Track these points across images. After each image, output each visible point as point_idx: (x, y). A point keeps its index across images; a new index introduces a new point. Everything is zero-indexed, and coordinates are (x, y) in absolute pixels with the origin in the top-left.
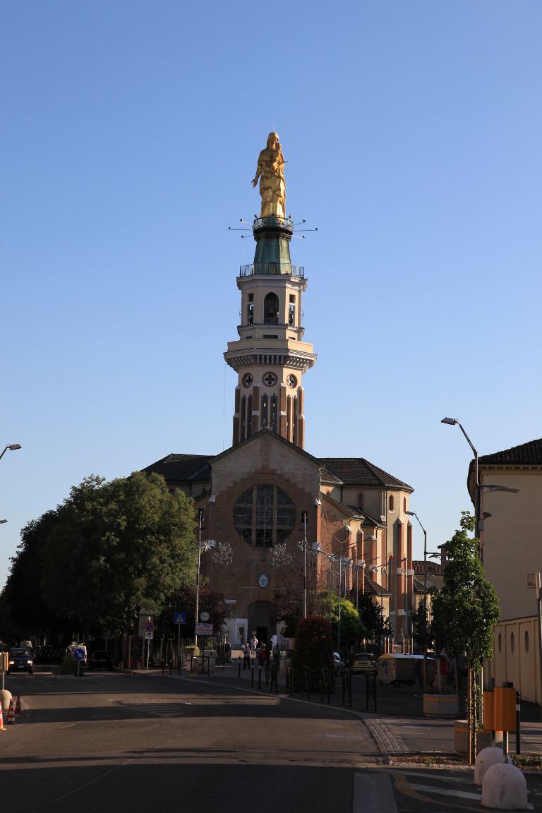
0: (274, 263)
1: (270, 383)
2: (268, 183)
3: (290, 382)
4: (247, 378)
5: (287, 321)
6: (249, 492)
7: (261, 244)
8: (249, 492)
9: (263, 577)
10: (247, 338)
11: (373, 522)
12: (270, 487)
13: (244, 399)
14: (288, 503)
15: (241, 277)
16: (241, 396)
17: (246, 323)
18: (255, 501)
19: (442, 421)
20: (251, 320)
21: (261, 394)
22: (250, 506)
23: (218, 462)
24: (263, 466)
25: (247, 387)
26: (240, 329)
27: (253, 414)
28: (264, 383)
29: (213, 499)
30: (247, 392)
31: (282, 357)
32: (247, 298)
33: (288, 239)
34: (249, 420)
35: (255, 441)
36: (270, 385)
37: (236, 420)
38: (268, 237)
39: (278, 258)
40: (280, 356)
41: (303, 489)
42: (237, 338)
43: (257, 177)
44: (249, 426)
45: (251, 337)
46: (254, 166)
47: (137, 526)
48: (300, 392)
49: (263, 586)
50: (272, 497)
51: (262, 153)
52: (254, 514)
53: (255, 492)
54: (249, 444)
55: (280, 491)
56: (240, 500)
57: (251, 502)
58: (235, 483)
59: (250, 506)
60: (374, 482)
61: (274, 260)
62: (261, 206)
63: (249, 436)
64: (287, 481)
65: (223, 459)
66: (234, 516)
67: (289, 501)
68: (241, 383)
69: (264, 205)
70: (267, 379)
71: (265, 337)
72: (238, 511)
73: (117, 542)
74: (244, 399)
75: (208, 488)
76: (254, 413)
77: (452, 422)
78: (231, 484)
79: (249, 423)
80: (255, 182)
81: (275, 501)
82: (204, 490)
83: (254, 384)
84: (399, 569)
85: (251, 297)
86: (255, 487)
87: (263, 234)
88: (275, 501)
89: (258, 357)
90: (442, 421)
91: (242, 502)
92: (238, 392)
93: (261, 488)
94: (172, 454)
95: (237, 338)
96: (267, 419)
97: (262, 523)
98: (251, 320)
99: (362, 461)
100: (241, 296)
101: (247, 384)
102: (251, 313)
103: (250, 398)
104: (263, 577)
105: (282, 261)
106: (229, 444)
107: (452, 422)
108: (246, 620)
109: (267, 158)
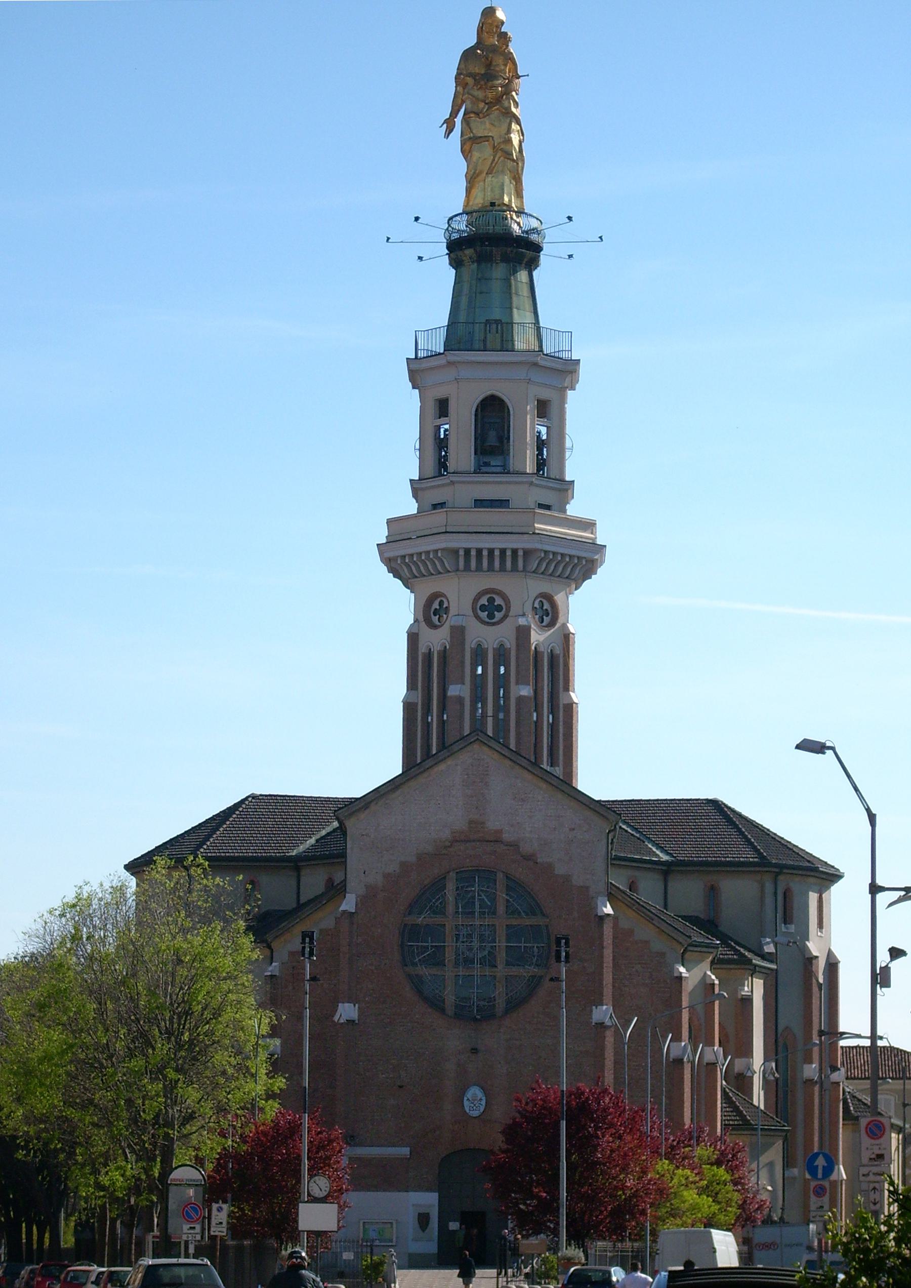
0: (498, 322)
1: (491, 616)
2: (481, 128)
3: (540, 613)
4: (436, 605)
5: (530, 467)
6: (438, 885)
7: (466, 277)
8: (438, 885)
9: (475, 1092)
10: (435, 506)
11: (744, 955)
12: (487, 875)
13: (429, 656)
14: (534, 914)
15: (416, 357)
16: (422, 649)
17: (430, 471)
18: (451, 909)
19: (798, 747)
20: (442, 465)
21: (470, 643)
22: (438, 919)
23: (362, 816)
24: (471, 822)
25: (435, 627)
26: (417, 488)
27: (449, 693)
28: (477, 617)
29: (349, 904)
30: (437, 639)
31: (521, 553)
32: (432, 410)
33: (532, 264)
34: (443, 708)
35: (449, 762)
36: (490, 622)
37: (409, 708)
38: (483, 259)
39: (509, 308)
40: (515, 552)
41: (567, 878)
42: (410, 507)
43: (454, 113)
44: (442, 724)
45: (442, 505)
46: (449, 88)
47: (548, 1197)
48: (567, 638)
49: (475, 1113)
50: (493, 899)
51: (468, 55)
52: (450, 942)
53: (451, 886)
54: (436, 769)
55: (513, 885)
56: (414, 907)
57: (441, 911)
58: (403, 864)
59: (438, 919)
60: (752, 857)
61: (496, 314)
62: (464, 184)
63: (442, 746)
64: (530, 858)
65: (373, 807)
66: (402, 946)
67: (535, 909)
68: (421, 618)
69: (472, 180)
70: (483, 608)
71: (480, 503)
72: (411, 933)
73: (22, 1151)
74: (429, 656)
75: (338, 877)
76: (454, 690)
77: (817, 748)
78: (393, 868)
79: (440, 716)
80: (449, 124)
81: (501, 909)
82: (330, 883)
83: (451, 620)
84: (806, 1067)
85: (442, 408)
86: (452, 875)
87: (469, 252)
88: (501, 909)
89: (462, 553)
90: (798, 747)
91: (509, 889)
92: (413, 638)
93: (466, 877)
94: (253, 796)
95: (410, 507)
96: (484, 707)
97: (468, 962)
98: (442, 465)
99: (716, 806)
100: (420, 404)
101: (435, 619)
102: (442, 444)
103: (444, 654)
104: (475, 1092)
105: (517, 318)
106: (393, 767)
107: (817, 748)
108: (435, 1196)
109: (479, 69)
